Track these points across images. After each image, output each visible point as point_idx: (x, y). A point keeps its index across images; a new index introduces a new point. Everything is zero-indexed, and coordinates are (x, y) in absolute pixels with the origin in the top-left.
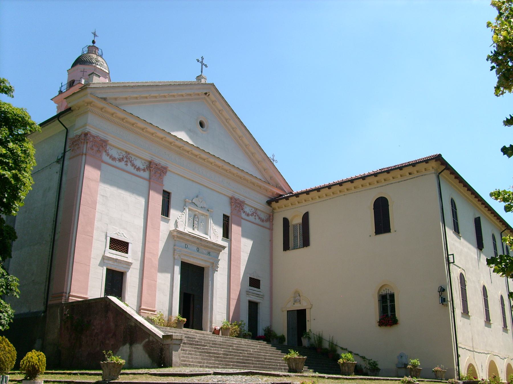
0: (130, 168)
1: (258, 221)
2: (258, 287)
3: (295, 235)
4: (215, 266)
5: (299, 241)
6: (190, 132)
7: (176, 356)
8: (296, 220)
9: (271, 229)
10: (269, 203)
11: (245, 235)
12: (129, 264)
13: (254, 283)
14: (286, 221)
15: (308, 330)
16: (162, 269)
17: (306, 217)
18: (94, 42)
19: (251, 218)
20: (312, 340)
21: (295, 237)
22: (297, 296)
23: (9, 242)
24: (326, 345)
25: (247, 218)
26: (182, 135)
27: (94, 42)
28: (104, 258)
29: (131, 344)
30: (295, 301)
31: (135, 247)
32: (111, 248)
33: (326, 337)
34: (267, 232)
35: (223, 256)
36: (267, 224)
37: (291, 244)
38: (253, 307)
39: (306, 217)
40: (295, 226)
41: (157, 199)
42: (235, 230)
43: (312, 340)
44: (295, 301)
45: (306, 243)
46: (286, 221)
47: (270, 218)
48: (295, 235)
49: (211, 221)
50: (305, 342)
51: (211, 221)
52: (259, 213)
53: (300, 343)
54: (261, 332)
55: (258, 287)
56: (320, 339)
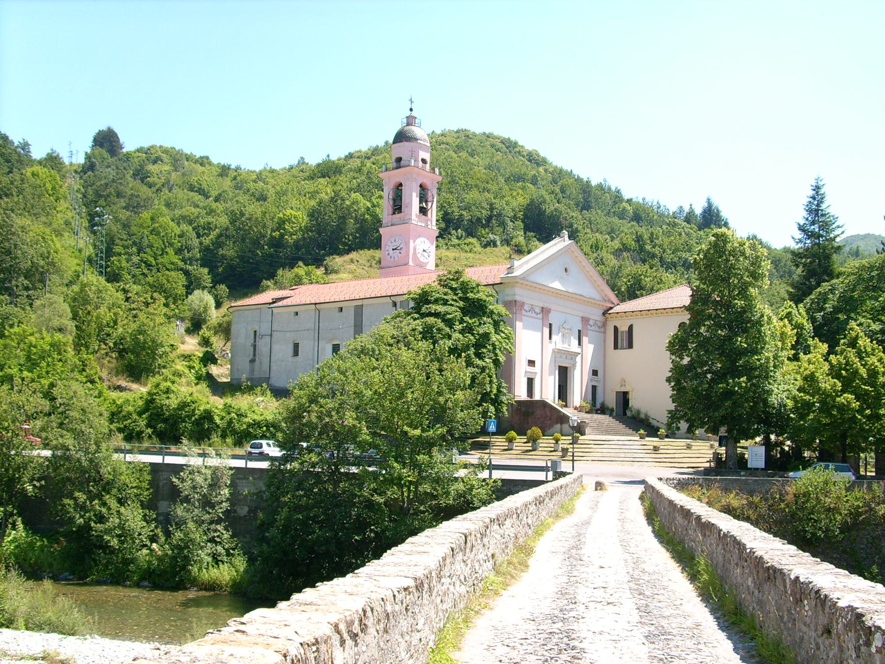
0: (534, 315)
1: (597, 329)
2: (597, 375)
3: (623, 340)
4: (574, 365)
5: (625, 344)
6: (561, 280)
7: (587, 431)
8: (623, 328)
9: (605, 333)
10: (604, 314)
11: (590, 342)
12: (536, 373)
13: (595, 373)
14: (616, 328)
15: (630, 406)
16: (550, 375)
17: (631, 328)
18: (411, 110)
19: (593, 328)
20: (634, 412)
21: (622, 340)
22: (623, 382)
23: (461, 357)
24: (642, 416)
25: (591, 328)
26: (556, 285)
27: (411, 110)
28: (526, 372)
29: (561, 424)
30: (622, 386)
31: (538, 364)
32: (529, 365)
33: (643, 411)
34: (602, 335)
35: (578, 359)
36: (602, 330)
37: (619, 346)
38: (594, 388)
39: (631, 328)
40: (622, 332)
41: (546, 331)
42: (585, 340)
43: (634, 412)
44: (622, 386)
45: (630, 346)
46: (616, 328)
47: (604, 325)
48: (623, 340)
49: (572, 338)
50: (629, 413)
51: (572, 338)
52: (597, 323)
53: (625, 414)
54: (598, 406)
55: (597, 375)
56: (639, 412)
